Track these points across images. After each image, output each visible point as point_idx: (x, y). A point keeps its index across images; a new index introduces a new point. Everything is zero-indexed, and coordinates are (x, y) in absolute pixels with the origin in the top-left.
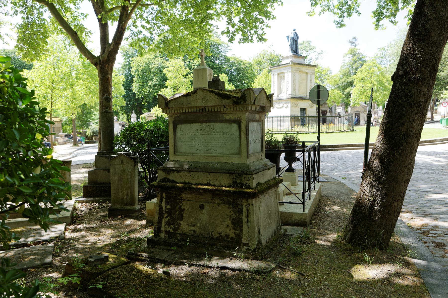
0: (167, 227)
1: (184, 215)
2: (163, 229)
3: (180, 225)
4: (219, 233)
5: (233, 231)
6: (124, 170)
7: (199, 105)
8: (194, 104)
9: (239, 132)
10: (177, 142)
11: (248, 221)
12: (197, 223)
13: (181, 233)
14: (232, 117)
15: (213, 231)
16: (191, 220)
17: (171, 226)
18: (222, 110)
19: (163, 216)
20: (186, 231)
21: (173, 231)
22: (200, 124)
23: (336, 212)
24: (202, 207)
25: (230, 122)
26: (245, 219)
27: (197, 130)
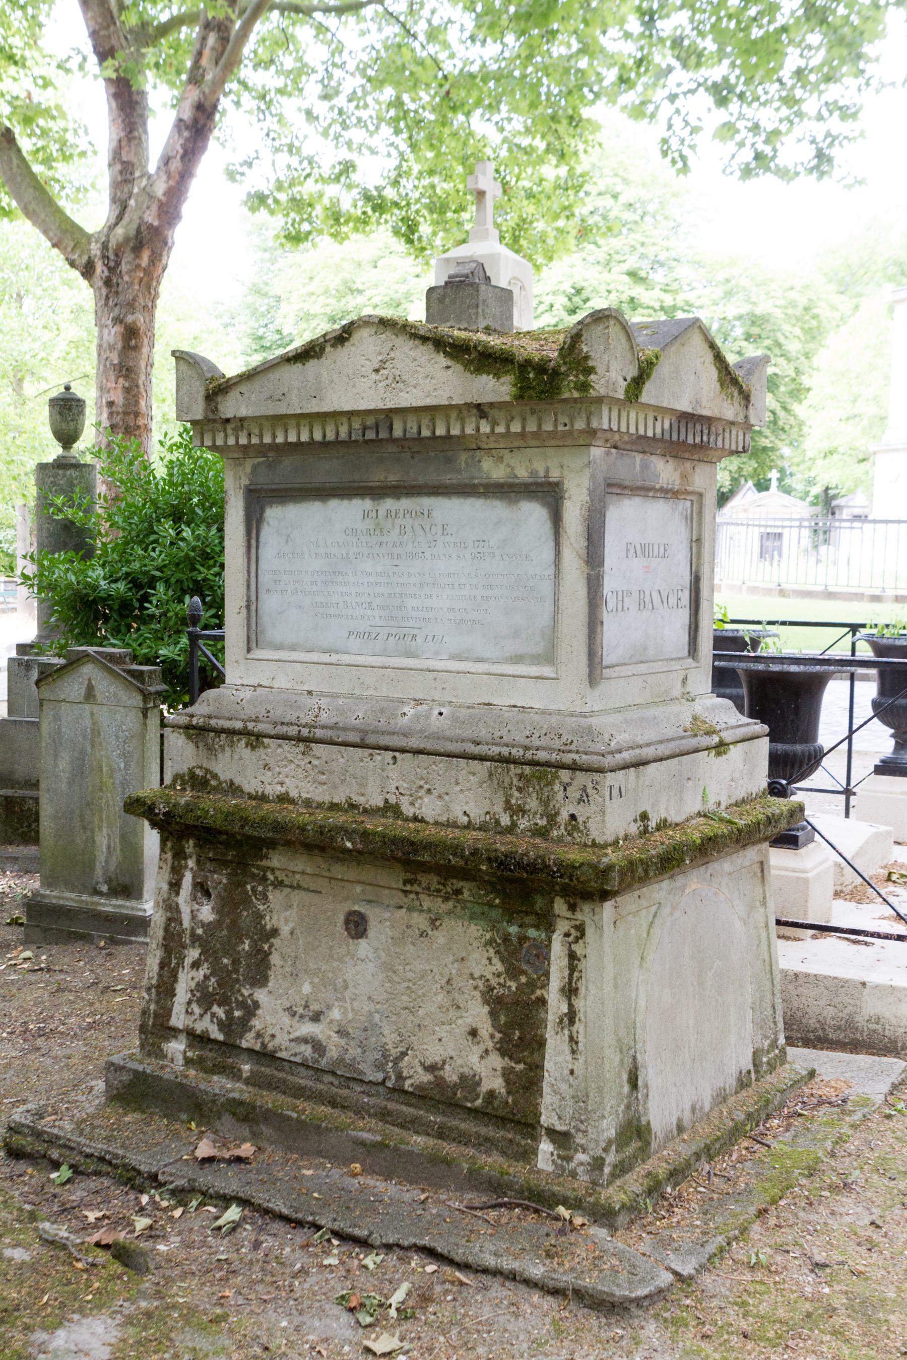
0: (197, 1010)
1: (275, 959)
2: (178, 1019)
3: (251, 1009)
4: (432, 1068)
5: (497, 1061)
6: (96, 730)
7: (363, 406)
8: (340, 399)
9: (552, 544)
10: (263, 595)
11: (572, 1016)
12: (329, 1007)
13: (257, 1047)
14: (521, 467)
15: (404, 1054)
16: (306, 988)
17: (215, 1008)
18: (469, 430)
19: (181, 960)
20: (282, 1040)
21: (221, 1037)
22: (368, 503)
23: (434, 1114)
24: (357, 926)
25: (509, 491)
26: (556, 1005)
27: (354, 532)
